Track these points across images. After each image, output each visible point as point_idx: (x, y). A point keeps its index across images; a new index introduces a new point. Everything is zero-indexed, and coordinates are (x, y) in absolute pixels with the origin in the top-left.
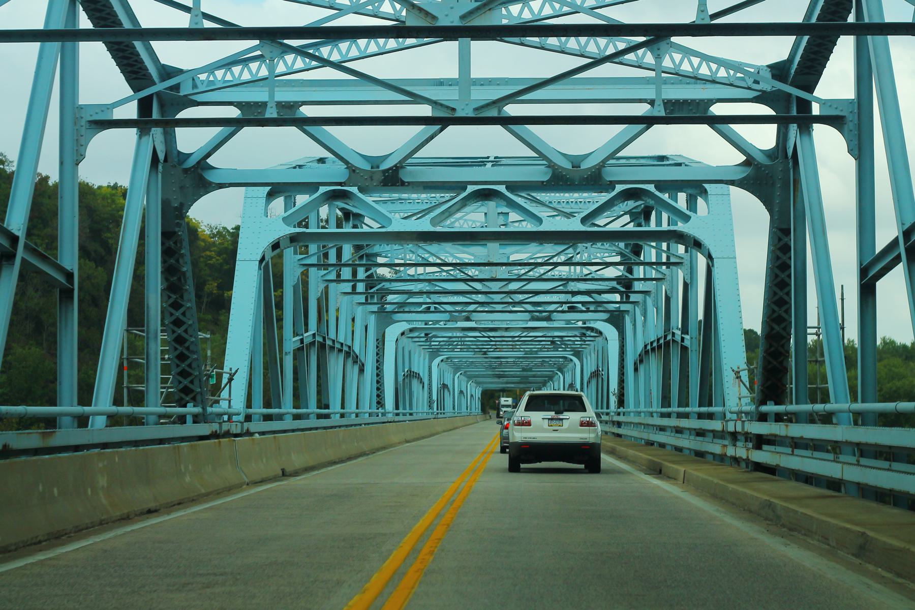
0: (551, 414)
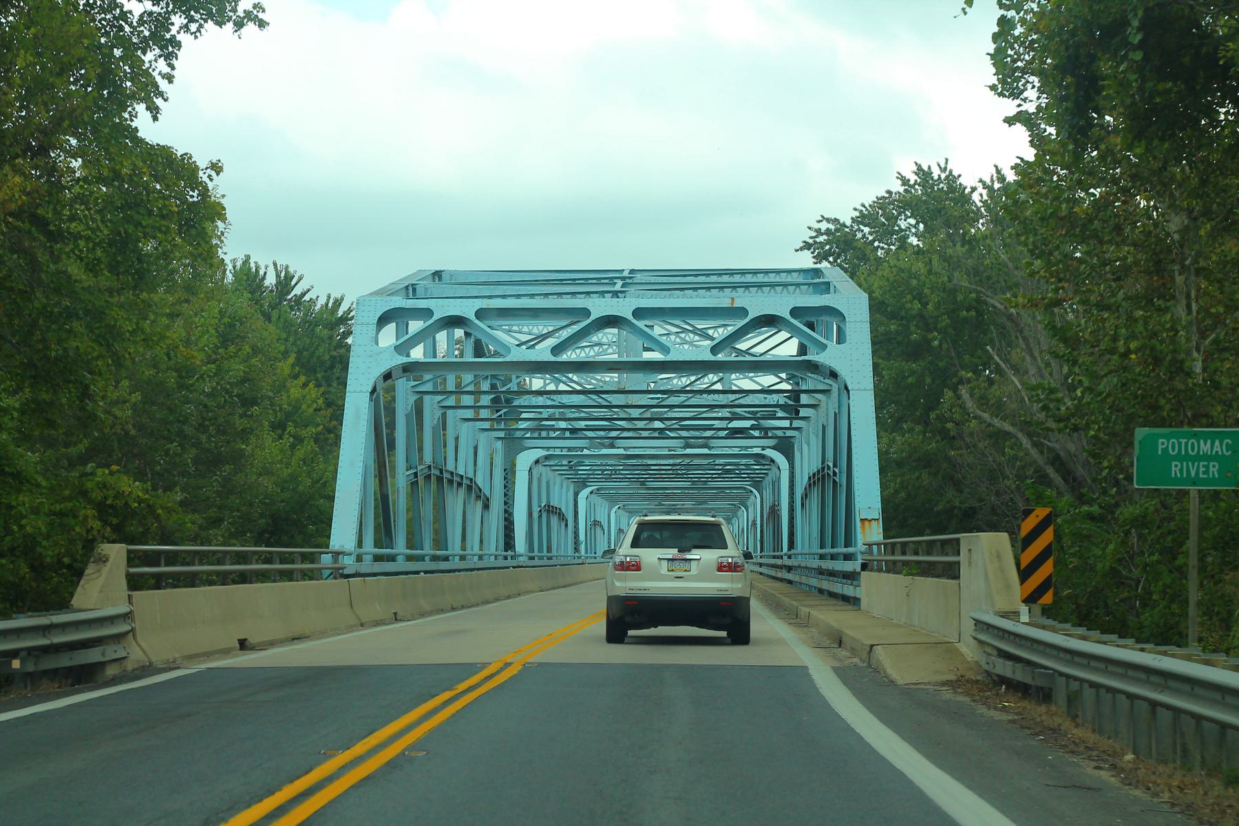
0: (672, 552)
